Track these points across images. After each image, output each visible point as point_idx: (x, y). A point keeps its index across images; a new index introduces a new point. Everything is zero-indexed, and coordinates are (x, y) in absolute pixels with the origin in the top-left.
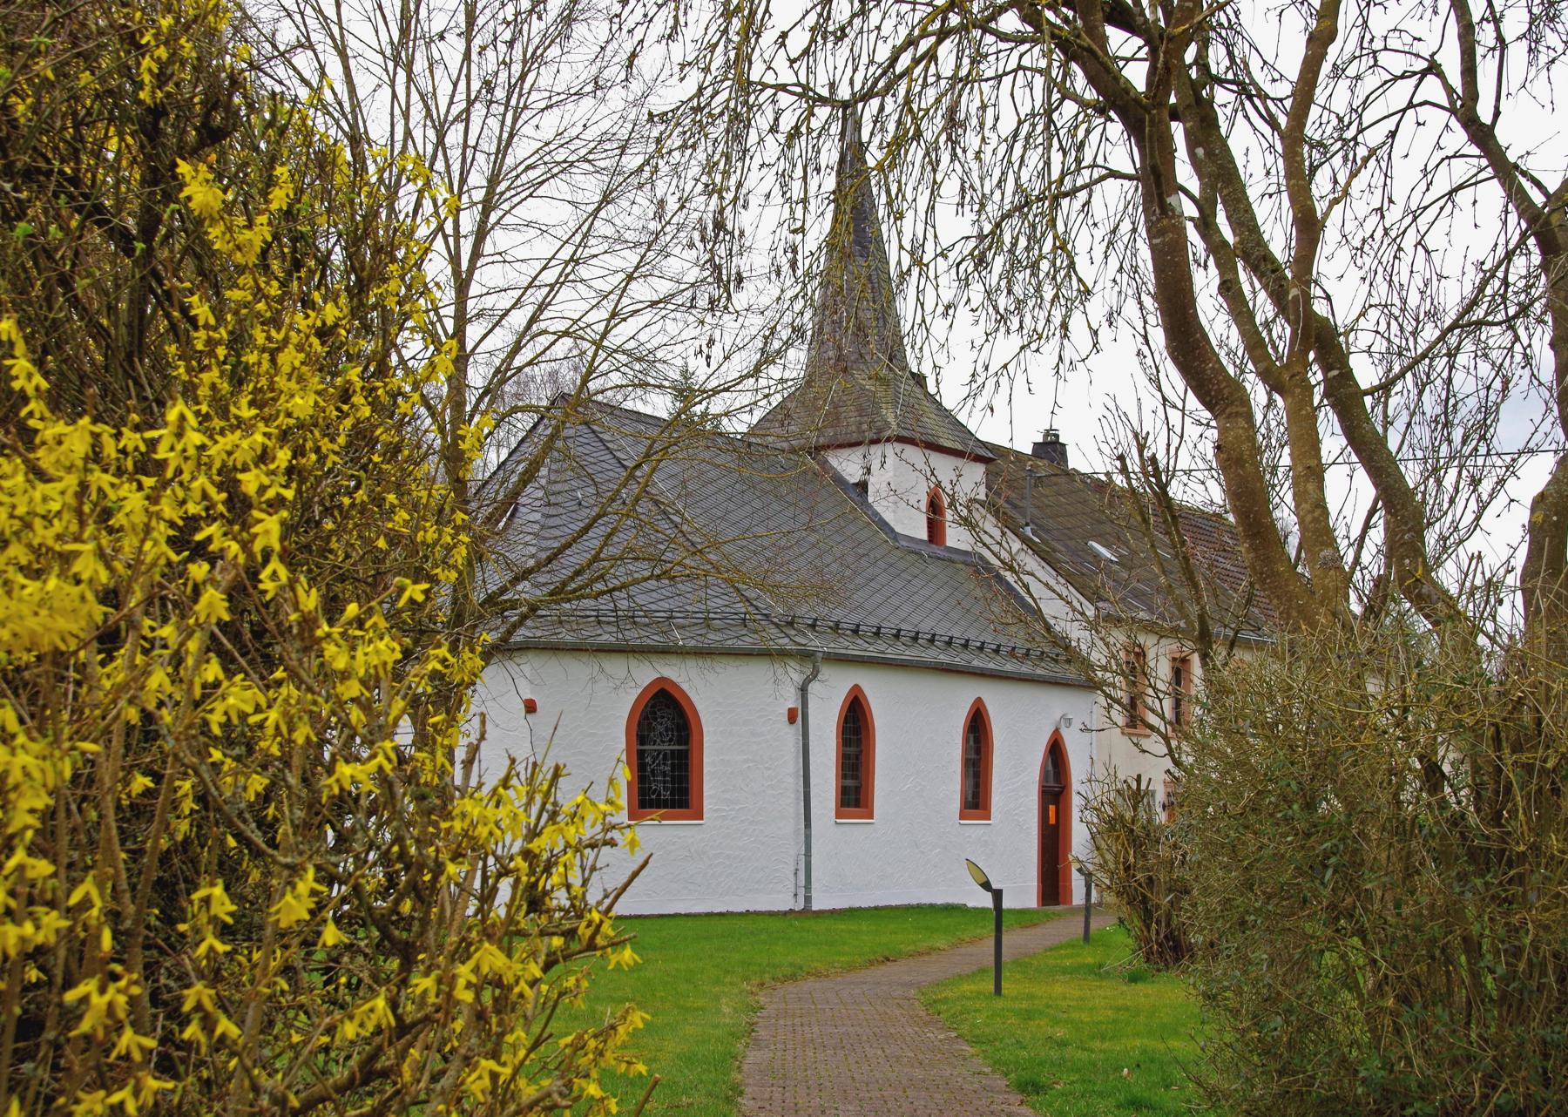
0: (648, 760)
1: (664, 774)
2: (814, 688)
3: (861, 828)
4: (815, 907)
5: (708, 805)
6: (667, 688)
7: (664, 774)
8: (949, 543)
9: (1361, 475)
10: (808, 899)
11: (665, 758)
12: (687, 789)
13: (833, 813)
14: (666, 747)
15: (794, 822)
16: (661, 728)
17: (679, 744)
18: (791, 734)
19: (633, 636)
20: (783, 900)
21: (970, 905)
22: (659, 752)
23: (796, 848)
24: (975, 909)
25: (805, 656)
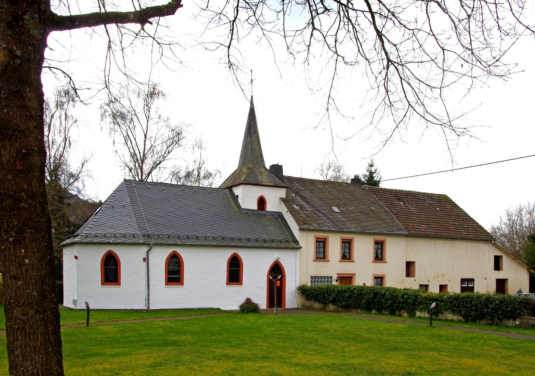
0: (108, 270)
1: (112, 274)
2: (150, 253)
3: (180, 288)
4: (151, 308)
5: (122, 282)
6: (175, 253)
7: (112, 274)
8: (267, 210)
9: (155, 182)
10: (149, 307)
11: (112, 270)
12: (105, 279)
13: (164, 284)
14: (113, 267)
15: (145, 286)
16: (111, 263)
17: (107, 268)
18: (144, 265)
19: (160, 241)
20: (143, 307)
21: (222, 309)
22: (111, 268)
23: (146, 293)
24: (224, 311)
25: (148, 244)
